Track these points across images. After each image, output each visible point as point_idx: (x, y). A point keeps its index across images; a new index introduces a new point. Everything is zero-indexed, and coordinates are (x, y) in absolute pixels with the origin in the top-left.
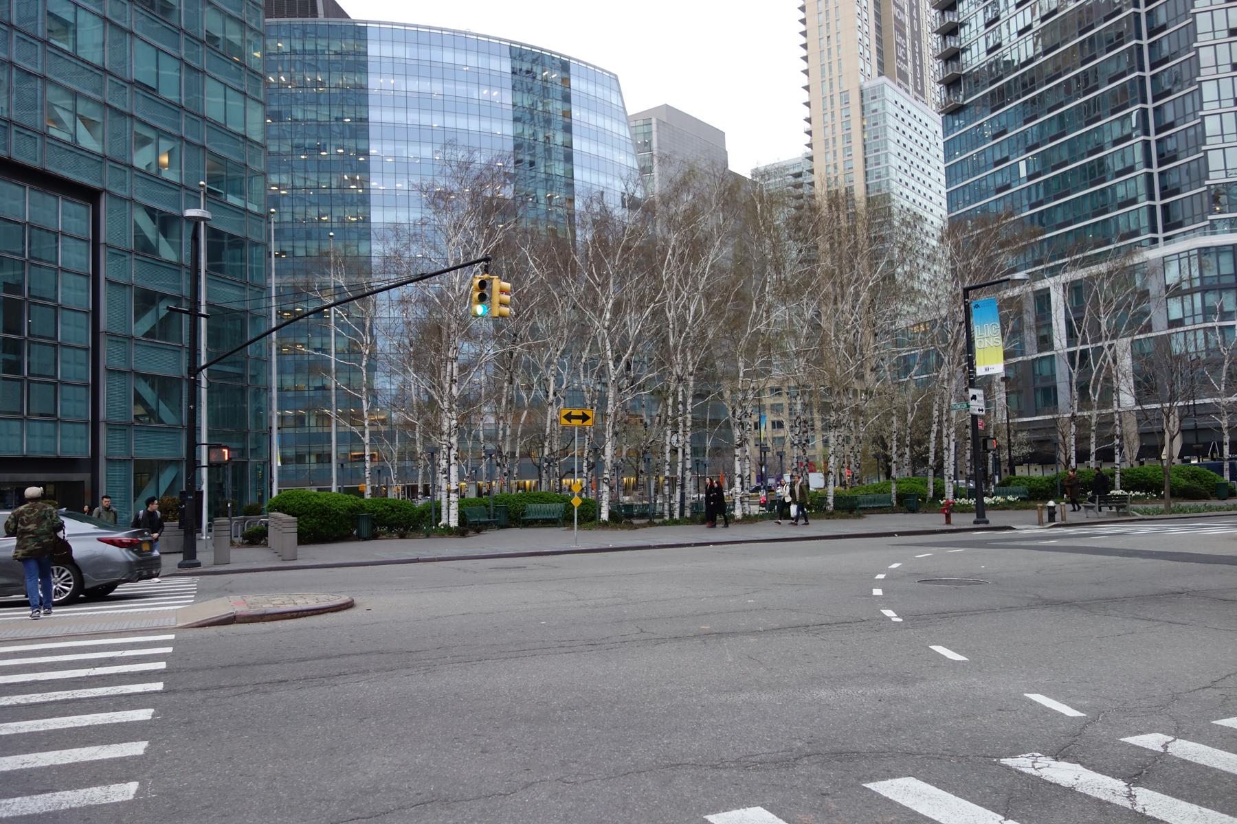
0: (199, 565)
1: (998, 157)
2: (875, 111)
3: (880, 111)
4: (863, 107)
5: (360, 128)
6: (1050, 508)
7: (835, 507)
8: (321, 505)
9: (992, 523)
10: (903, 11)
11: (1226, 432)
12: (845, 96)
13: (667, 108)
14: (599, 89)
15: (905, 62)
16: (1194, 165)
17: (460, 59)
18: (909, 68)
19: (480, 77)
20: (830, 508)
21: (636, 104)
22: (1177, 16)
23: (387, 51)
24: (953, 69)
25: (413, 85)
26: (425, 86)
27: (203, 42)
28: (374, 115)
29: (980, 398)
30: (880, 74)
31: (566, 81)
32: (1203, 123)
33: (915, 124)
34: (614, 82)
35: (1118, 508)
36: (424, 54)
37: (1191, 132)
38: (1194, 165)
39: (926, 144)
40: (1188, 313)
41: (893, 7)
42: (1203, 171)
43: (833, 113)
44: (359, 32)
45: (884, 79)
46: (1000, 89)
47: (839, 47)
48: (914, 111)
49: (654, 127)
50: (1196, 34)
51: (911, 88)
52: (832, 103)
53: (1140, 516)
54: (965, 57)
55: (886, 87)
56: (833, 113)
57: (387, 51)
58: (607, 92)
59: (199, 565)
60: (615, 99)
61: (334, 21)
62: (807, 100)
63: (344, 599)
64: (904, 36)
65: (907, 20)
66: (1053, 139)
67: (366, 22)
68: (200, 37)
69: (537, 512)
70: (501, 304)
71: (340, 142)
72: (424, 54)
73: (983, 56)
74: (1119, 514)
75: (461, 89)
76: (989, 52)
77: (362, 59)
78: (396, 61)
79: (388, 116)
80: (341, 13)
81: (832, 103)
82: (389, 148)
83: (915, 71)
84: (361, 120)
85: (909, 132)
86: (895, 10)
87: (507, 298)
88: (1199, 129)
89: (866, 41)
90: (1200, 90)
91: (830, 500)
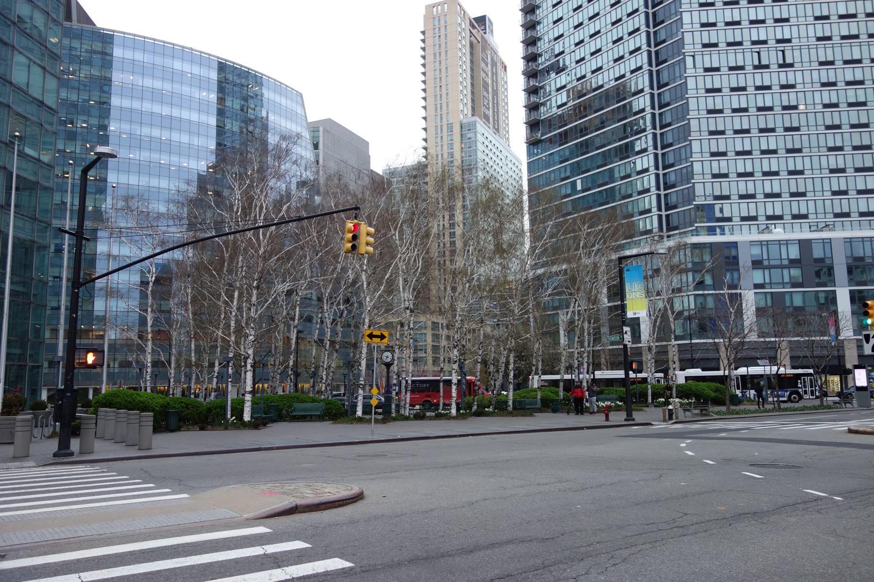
0: (72, 454)
1: (563, 176)
2: (470, 138)
3: (473, 139)
4: (462, 135)
5: (104, 109)
6: (670, 410)
8: (143, 403)
9: (638, 421)
10: (487, 75)
12: (450, 127)
13: (329, 121)
14: (289, 102)
15: (488, 109)
16: (686, 191)
17: (187, 67)
18: (490, 113)
19: (200, 82)
20: (510, 408)
21: (313, 116)
22: (676, 98)
23: (129, 54)
24: (534, 116)
26: (158, 84)
27: (14, 23)
29: (629, 333)
30: (473, 115)
31: (221, 100)
32: (692, 166)
33: (494, 150)
34: (299, 98)
35: (702, 411)
36: (158, 60)
37: (684, 171)
38: (686, 191)
39: (501, 164)
41: (482, 72)
42: (691, 196)
43: (442, 137)
44: (106, 38)
45: (477, 118)
46: (566, 131)
47: (447, 94)
48: (494, 142)
49: (321, 133)
50: (688, 110)
51: (491, 126)
52: (442, 130)
53: (716, 417)
55: (478, 124)
56: (442, 137)
57: (129, 54)
58: (294, 105)
59: (72, 454)
60: (299, 111)
61: (86, 27)
62: (424, 126)
63: (355, 490)
64: (488, 92)
65: (490, 81)
66: (598, 167)
67: (114, 31)
68: (12, 18)
70: (367, 244)
71: (85, 118)
72: (158, 60)
74: (702, 415)
75: (186, 90)
77: (108, 58)
78: (136, 63)
79: (126, 103)
80: (89, 21)
81: (442, 130)
82: (125, 127)
83: (494, 115)
84: (104, 103)
85: (491, 155)
86: (483, 75)
87: (372, 240)
88: (689, 169)
89: (465, 92)
90: (690, 145)
91: (510, 403)
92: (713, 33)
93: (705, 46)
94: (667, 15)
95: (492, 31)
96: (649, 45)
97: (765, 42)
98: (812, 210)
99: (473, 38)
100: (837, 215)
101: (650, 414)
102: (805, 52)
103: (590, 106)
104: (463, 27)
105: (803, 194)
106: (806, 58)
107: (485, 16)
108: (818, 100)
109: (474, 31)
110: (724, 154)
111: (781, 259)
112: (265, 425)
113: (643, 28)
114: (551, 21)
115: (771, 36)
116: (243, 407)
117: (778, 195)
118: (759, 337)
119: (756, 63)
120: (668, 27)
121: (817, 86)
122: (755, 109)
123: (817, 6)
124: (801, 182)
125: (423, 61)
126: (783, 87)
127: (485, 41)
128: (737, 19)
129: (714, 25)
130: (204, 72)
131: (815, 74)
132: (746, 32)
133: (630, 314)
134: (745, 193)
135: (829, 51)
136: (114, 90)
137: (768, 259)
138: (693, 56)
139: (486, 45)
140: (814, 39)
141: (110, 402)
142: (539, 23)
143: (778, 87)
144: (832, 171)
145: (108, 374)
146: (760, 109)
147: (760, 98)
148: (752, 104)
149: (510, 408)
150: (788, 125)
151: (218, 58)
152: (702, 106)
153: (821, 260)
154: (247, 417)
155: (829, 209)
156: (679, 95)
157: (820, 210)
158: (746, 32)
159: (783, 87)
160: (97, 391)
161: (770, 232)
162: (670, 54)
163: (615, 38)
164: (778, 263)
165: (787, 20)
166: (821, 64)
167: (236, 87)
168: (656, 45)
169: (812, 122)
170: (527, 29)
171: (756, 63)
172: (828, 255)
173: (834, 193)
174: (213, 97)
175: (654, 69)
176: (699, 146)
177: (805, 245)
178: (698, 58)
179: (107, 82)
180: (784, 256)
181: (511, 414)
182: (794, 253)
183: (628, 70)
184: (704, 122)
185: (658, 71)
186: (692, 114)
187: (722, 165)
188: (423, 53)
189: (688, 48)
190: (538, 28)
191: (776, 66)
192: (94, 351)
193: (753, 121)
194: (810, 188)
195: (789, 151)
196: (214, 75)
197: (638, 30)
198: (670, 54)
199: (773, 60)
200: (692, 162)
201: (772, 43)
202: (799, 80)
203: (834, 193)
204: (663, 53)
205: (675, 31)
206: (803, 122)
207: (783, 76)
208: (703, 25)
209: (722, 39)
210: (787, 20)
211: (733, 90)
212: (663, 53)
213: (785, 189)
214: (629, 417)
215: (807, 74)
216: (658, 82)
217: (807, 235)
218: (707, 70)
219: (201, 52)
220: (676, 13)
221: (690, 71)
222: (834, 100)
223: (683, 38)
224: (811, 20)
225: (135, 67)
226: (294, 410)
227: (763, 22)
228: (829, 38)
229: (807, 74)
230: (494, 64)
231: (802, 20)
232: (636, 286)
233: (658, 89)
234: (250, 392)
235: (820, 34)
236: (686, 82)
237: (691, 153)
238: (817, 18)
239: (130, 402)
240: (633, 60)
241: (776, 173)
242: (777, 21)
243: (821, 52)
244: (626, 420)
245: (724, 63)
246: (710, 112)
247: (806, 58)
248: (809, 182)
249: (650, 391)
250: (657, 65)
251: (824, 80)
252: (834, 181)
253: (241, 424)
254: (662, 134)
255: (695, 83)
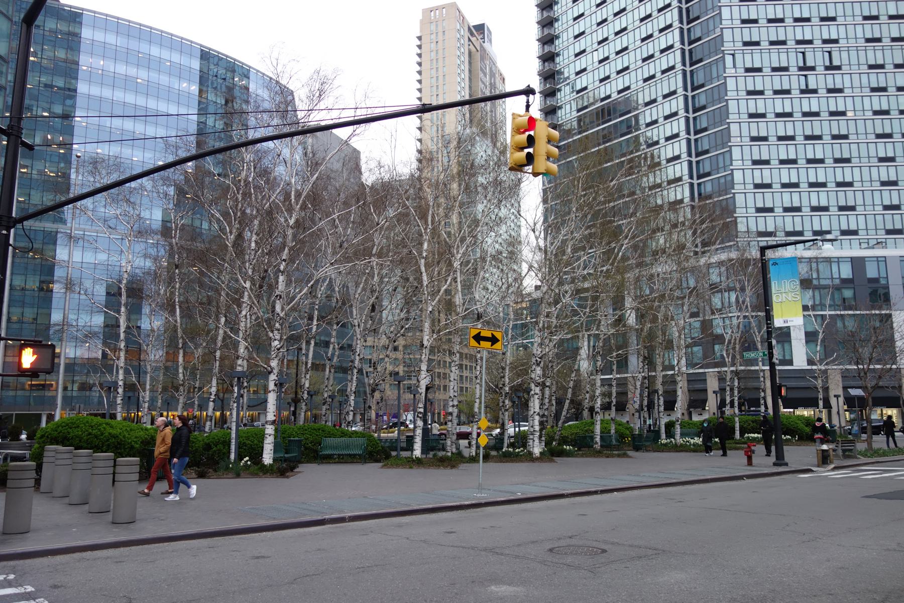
7: (601, 446)
8: (115, 437)
11: (821, 390)
17: (166, 54)
19: (179, 72)
20: (597, 447)
25: (121, 69)
26: (132, 71)
28: (82, 88)
32: (732, 174)
36: (133, 44)
37: (722, 180)
40: (726, 305)
41: (480, 83)
44: (75, 17)
54: (560, 113)
57: (99, 36)
67: (83, 9)
69: (335, 448)
72: (133, 44)
73: (575, 114)
76: (579, 111)
88: (729, 178)
90: (730, 151)
92: (755, 31)
93: (746, 44)
94: (703, 10)
95: (490, 41)
96: (683, 43)
97: (810, 42)
98: (862, 226)
99: (472, 47)
100: (889, 232)
101: (798, 454)
102: (853, 54)
103: (615, 111)
104: (462, 33)
105: (853, 208)
106: (854, 61)
107: (483, 25)
108: (867, 106)
109: (473, 39)
110: (767, 162)
111: (832, 278)
112: (292, 469)
113: (676, 24)
114: (570, 17)
115: (817, 36)
116: (263, 443)
117: (826, 209)
118: (808, 364)
119: (801, 64)
120: (705, 24)
121: (866, 91)
122: (800, 115)
123: (865, 5)
124: (850, 195)
125: (418, 68)
126: (830, 91)
127: (483, 49)
128: (780, 16)
129: (755, 21)
130: (185, 61)
131: (864, 78)
132: (790, 30)
133: (778, 322)
134: (790, 205)
135: (879, 54)
136: (81, 75)
137: (818, 278)
138: (733, 55)
139: (484, 54)
140: (863, 40)
141: (61, 436)
142: (557, 20)
143: (825, 91)
144: (884, 184)
145: (64, 398)
146: (805, 114)
147: (805, 102)
148: (797, 108)
149: (597, 447)
150: (835, 132)
151: (201, 46)
152: (743, 110)
153: (876, 280)
154: (268, 458)
155: (880, 225)
156: (716, 97)
157: (871, 225)
158: (790, 30)
159: (830, 91)
160: (50, 417)
161: (819, 248)
162: (706, 52)
163: (644, 36)
164: (829, 282)
165: (833, 19)
166: (871, 67)
167: (220, 78)
168: (690, 43)
169: (861, 130)
170: (543, 27)
171: (801, 64)
172: (883, 274)
173: (886, 208)
174: (195, 88)
175: (688, 69)
176: (740, 155)
177: (858, 263)
178: (739, 57)
179: (71, 93)
180: (836, 275)
181: (598, 454)
182: (846, 272)
183: (658, 69)
184: (745, 126)
185: (691, 71)
186: (733, 117)
187: (765, 175)
188: (418, 60)
189: (728, 46)
190: (556, 25)
191: (823, 68)
192: (35, 345)
193: (798, 127)
194: (860, 201)
195: (837, 161)
196: (196, 64)
197: (670, 26)
198: (706, 52)
199: (819, 62)
200: (732, 170)
201: (818, 43)
202: (847, 84)
203: (886, 208)
204: (698, 54)
205: (711, 28)
206: (852, 130)
207: (830, 79)
208: (744, 22)
209: (764, 37)
210: (833, 19)
211: (776, 92)
212: (698, 54)
213: (833, 202)
214: (780, 460)
215: (856, 78)
216: (692, 83)
217: (857, 253)
218: (748, 70)
219: (182, 38)
220: (713, 8)
221: (730, 71)
222: (885, 107)
223: (722, 35)
224: (859, 19)
225: (105, 50)
226: (326, 448)
227: (808, 20)
228: (879, 40)
229: (856, 78)
230: (492, 75)
231: (849, 19)
232: (787, 285)
233: (692, 91)
234: (273, 423)
235: (869, 36)
236: (725, 83)
237: (731, 160)
238: (866, 18)
239: (96, 437)
240: (664, 59)
241: (824, 185)
242: (823, 19)
243: (870, 54)
244: (775, 464)
245: (766, 64)
246: (751, 116)
247: (854, 61)
248: (859, 195)
249: (737, 425)
250: (691, 65)
251: (874, 85)
252: (886, 194)
253: (258, 469)
254: (696, 140)
255: (736, 84)
